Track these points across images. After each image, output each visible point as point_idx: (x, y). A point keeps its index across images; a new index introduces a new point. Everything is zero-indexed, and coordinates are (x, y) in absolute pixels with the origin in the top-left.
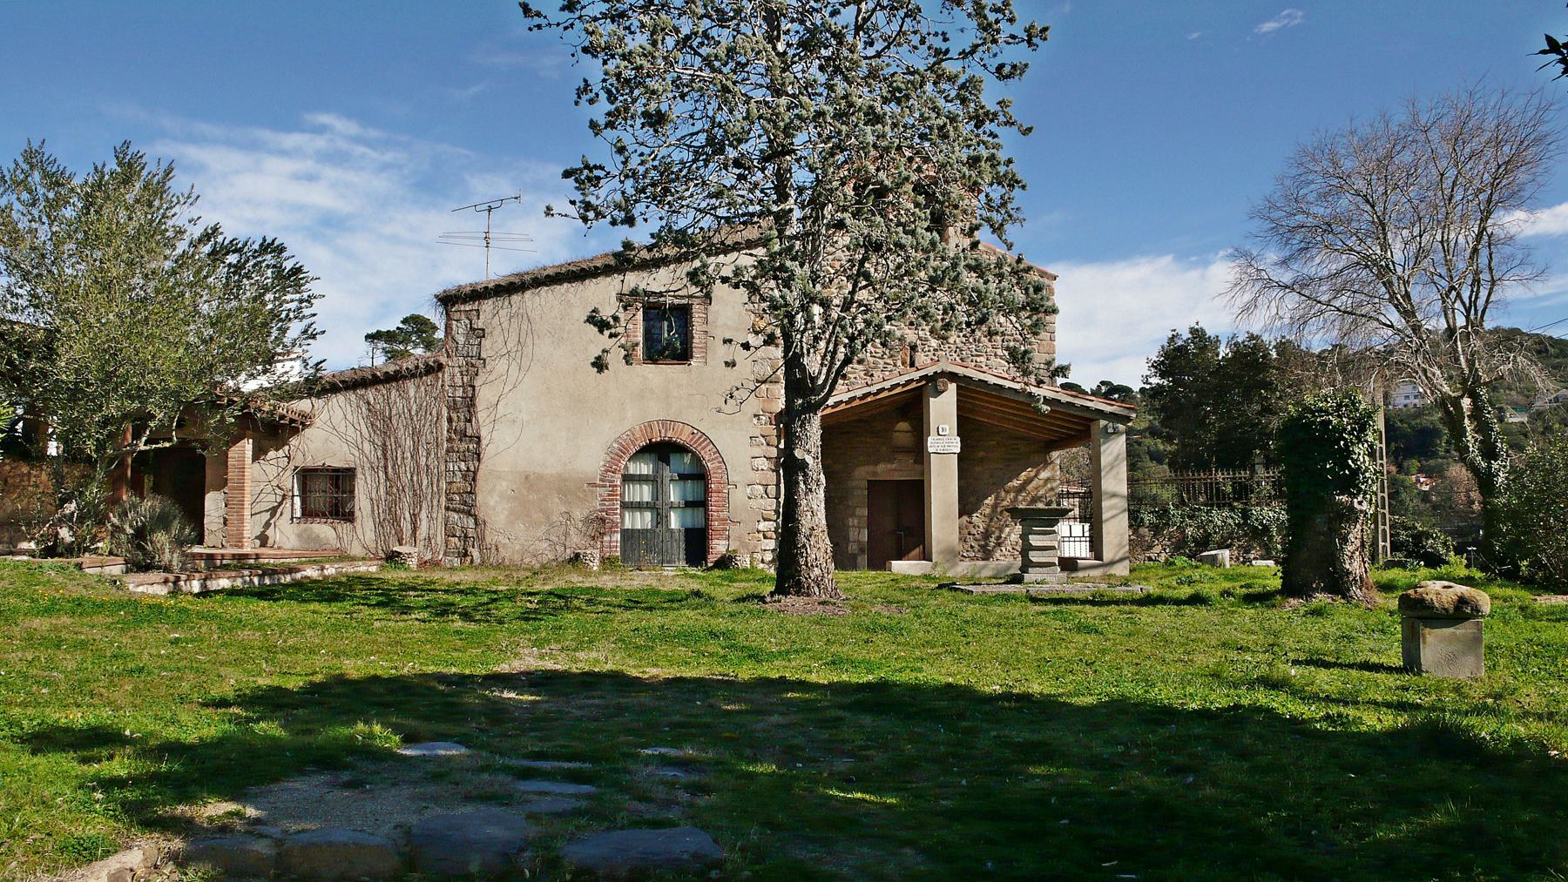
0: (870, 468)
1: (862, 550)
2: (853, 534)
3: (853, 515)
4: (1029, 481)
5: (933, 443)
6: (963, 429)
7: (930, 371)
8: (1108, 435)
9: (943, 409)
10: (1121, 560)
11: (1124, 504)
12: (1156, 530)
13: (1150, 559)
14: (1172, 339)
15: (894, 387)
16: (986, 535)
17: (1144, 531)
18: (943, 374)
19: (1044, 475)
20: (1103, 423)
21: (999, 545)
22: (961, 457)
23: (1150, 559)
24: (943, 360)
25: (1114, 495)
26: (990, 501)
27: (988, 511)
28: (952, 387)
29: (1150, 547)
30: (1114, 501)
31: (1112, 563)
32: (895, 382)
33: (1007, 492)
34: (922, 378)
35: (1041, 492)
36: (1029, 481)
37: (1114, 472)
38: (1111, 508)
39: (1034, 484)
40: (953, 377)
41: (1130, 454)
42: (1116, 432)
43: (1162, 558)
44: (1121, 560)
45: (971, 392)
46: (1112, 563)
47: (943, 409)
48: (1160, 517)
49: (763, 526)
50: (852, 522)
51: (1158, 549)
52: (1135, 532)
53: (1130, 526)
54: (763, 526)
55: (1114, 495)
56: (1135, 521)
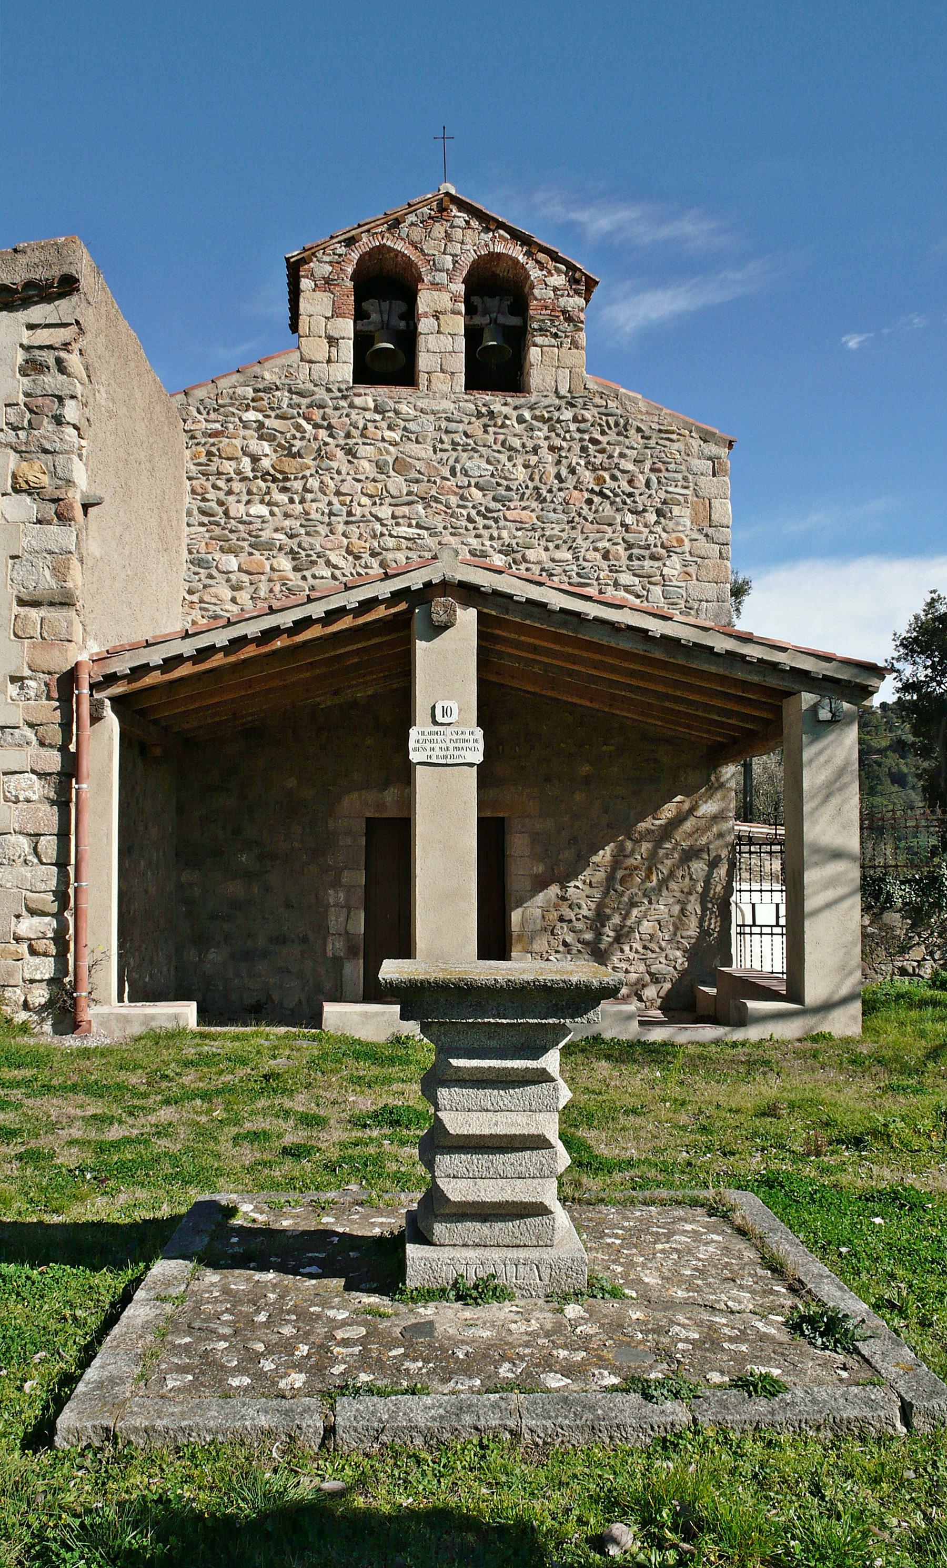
0: (371, 796)
1: (352, 951)
2: (335, 921)
3: (336, 883)
4: (678, 820)
5: (421, 743)
6: (489, 714)
7: (415, 581)
8: (820, 728)
9: (446, 672)
10: (846, 1000)
11: (855, 873)
12: (916, 916)
13: (903, 972)
14: (932, 604)
15: (333, 615)
16: (599, 919)
17: (893, 918)
18: (446, 587)
19: (708, 808)
20: (808, 699)
21: (618, 939)
22: (485, 773)
23: (903, 972)
24: (445, 555)
25: (837, 855)
26: (604, 855)
27: (601, 875)
28: (467, 618)
29: (904, 949)
30: (838, 867)
31: (827, 1007)
32: (334, 603)
33: (637, 842)
34: (398, 595)
35: (704, 840)
36: (678, 820)
37: (835, 801)
38: (832, 882)
39: (688, 825)
40: (468, 593)
41: (864, 753)
42: (836, 721)
43: (927, 971)
44: (846, 1000)
45: (502, 622)
46: (827, 1007)
47: (446, 672)
48: (924, 891)
49: (28, 926)
50: (335, 896)
51: (918, 953)
52: (876, 918)
53: (866, 909)
54: (28, 926)
55: (837, 855)
56: (873, 892)
